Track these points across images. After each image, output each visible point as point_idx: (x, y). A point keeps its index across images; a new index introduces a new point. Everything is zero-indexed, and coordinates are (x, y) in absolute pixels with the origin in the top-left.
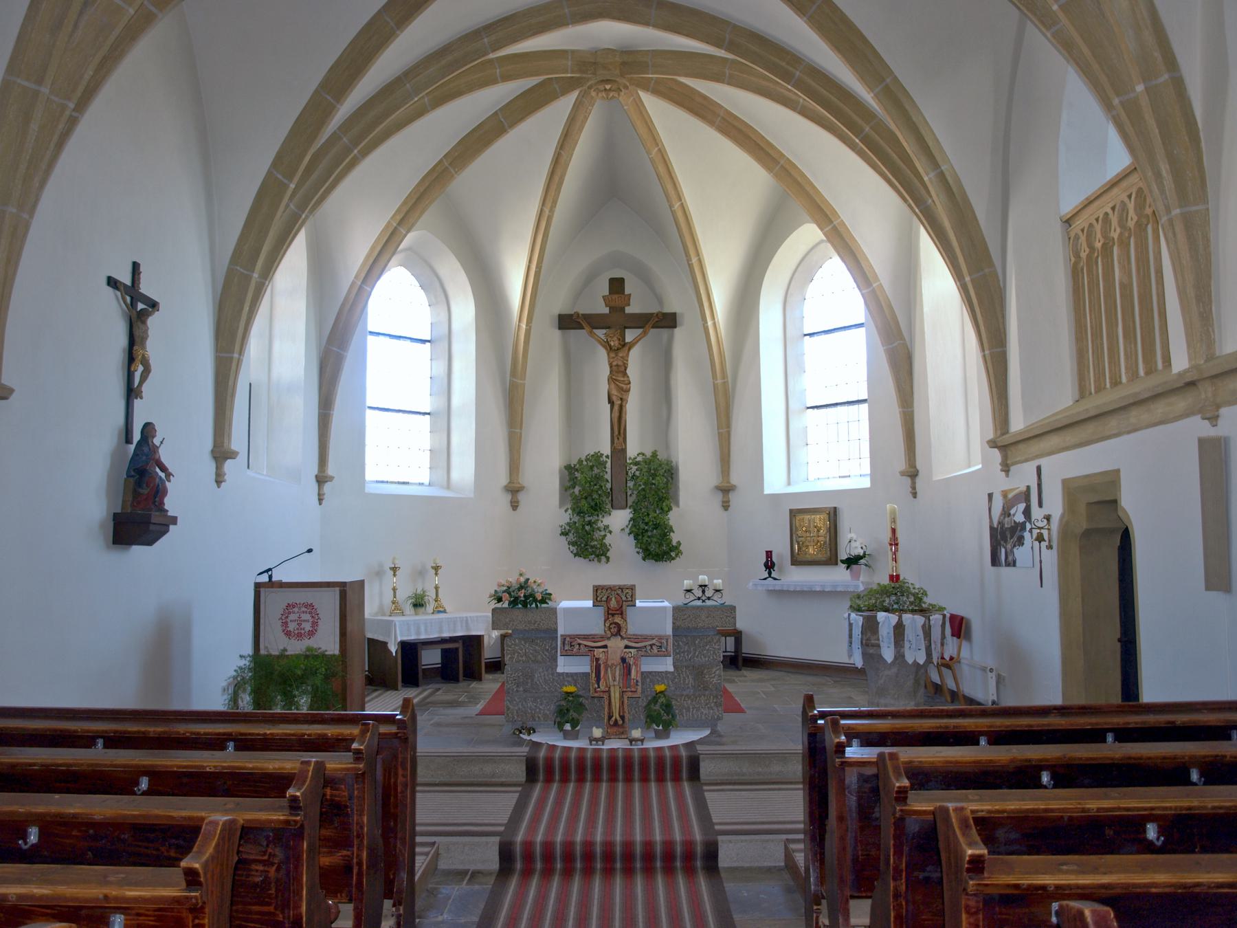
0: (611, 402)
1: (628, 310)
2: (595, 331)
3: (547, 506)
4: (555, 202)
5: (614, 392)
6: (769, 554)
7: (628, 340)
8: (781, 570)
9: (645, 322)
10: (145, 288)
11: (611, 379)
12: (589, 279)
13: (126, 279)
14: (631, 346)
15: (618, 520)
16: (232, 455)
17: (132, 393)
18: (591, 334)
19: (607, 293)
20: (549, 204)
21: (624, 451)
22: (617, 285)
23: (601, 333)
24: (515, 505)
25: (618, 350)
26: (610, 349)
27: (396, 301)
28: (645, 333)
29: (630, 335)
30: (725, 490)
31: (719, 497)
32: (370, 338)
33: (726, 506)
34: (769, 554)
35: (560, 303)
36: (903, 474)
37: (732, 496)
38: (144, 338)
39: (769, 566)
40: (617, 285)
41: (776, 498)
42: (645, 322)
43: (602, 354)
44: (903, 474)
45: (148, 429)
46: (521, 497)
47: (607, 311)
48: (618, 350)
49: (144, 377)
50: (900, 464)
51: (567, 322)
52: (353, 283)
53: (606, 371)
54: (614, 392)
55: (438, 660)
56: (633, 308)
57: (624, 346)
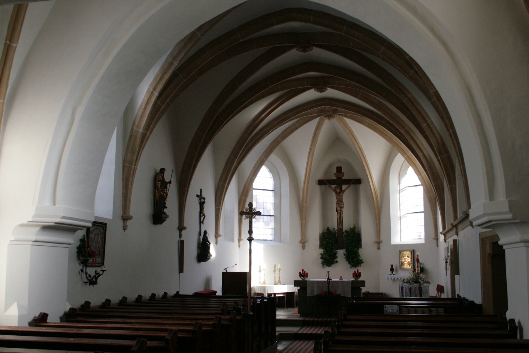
0: (337, 211)
1: (343, 178)
2: (331, 186)
3: (315, 250)
4: (312, 157)
5: (339, 208)
6: (392, 266)
7: (343, 189)
8: (396, 271)
9: (348, 182)
10: (203, 195)
11: (337, 203)
12: (330, 166)
13: (199, 194)
14: (344, 191)
15: (341, 253)
16: (220, 236)
17: (201, 222)
18: (330, 187)
19: (336, 172)
20: (311, 155)
21: (342, 229)
22: (339, 169)
23: (333, 186)
24: (304, 248)
25: (339, 193)
26: (336, 193)
27: (264, 179)
28: (349, 187)
29: (344, 187)
30: (379, 243)
31: (376, 245)
32: (254, 191)
33: (379, 248)
34: (392, 266)
35: (320, 176)
36: (434, 239)
37: (381, 245)
38: (205, 209)
39: (392, 270)
40: (339, 169)
41: (396, 246)
42: (348, 182)
43: (334, 194)
44: (434, 239)
45: (205, 232)
46: (306, 244)
47: (335, 178)
48: (339, 193)
49: (204, 219)
50: (433, 236)
51: (321, 182)
52: (249, 176)
53: (335, 200)
54: (339, 208)
55: (277, 313)
56: (345, 177)
57: (342, 191)
